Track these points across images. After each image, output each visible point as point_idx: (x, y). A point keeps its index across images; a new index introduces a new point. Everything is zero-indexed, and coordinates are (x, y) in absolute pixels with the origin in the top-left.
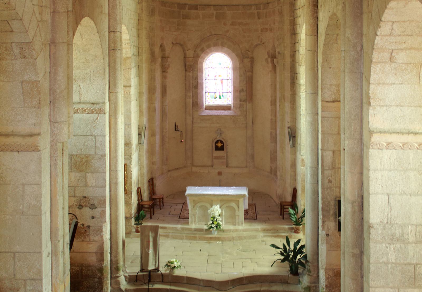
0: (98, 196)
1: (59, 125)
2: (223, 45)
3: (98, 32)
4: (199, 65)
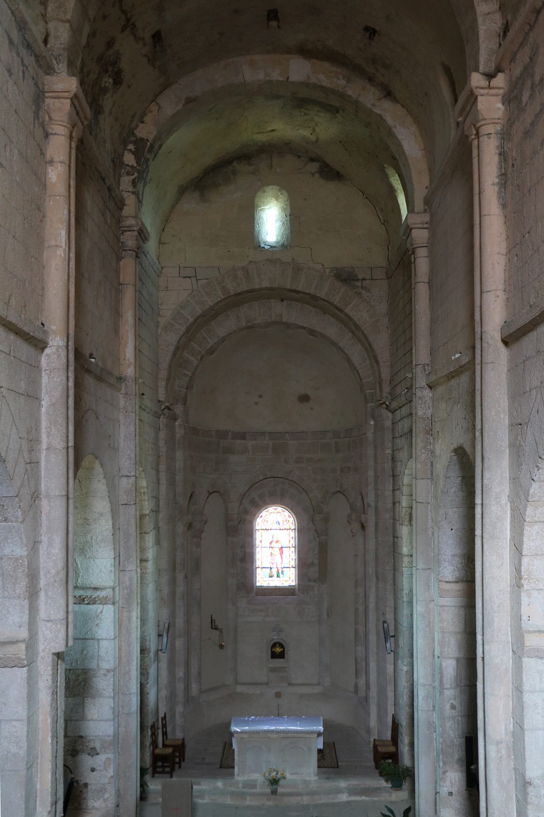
0: (101, 734)
1: (53, 625)
3: (105, 477)
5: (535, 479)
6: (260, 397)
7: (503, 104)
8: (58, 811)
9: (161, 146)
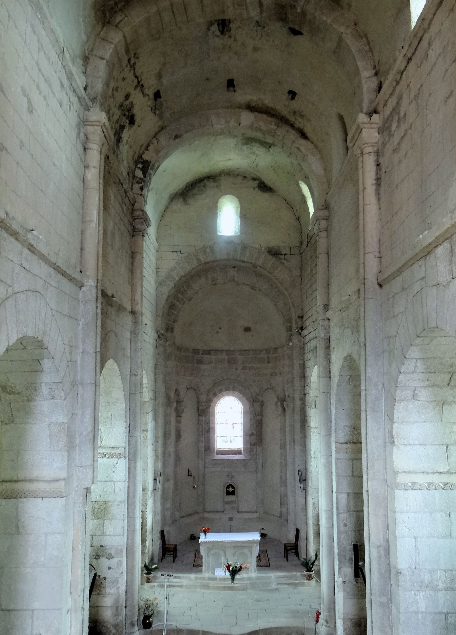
0: (115, 544)
2: (234, 389)
4: (211, 410)
5: (402, 372)
6: (220, 328)
7: (379, 133)
8: (85, 595)
9: (159, 166)
